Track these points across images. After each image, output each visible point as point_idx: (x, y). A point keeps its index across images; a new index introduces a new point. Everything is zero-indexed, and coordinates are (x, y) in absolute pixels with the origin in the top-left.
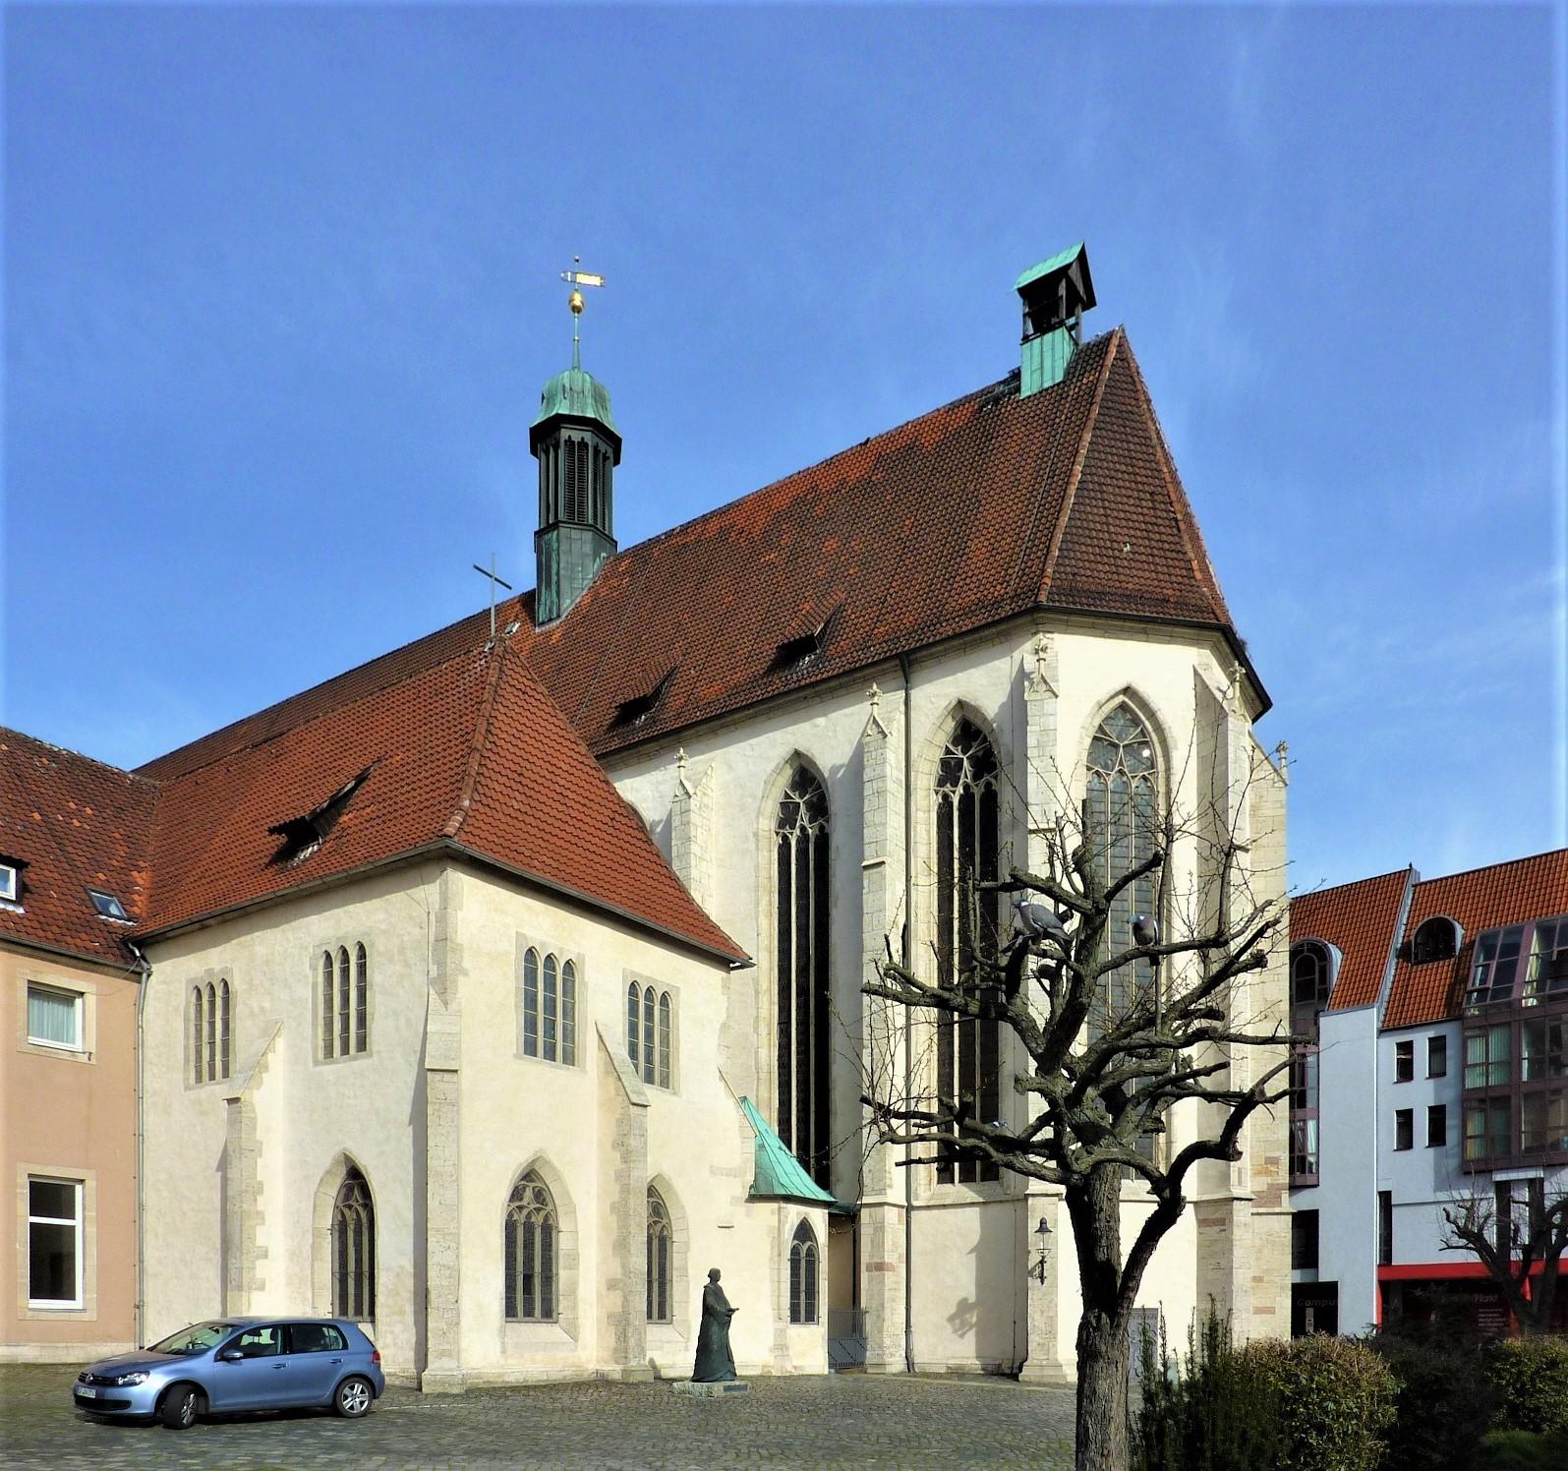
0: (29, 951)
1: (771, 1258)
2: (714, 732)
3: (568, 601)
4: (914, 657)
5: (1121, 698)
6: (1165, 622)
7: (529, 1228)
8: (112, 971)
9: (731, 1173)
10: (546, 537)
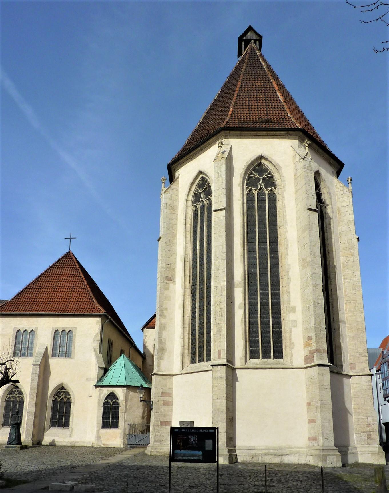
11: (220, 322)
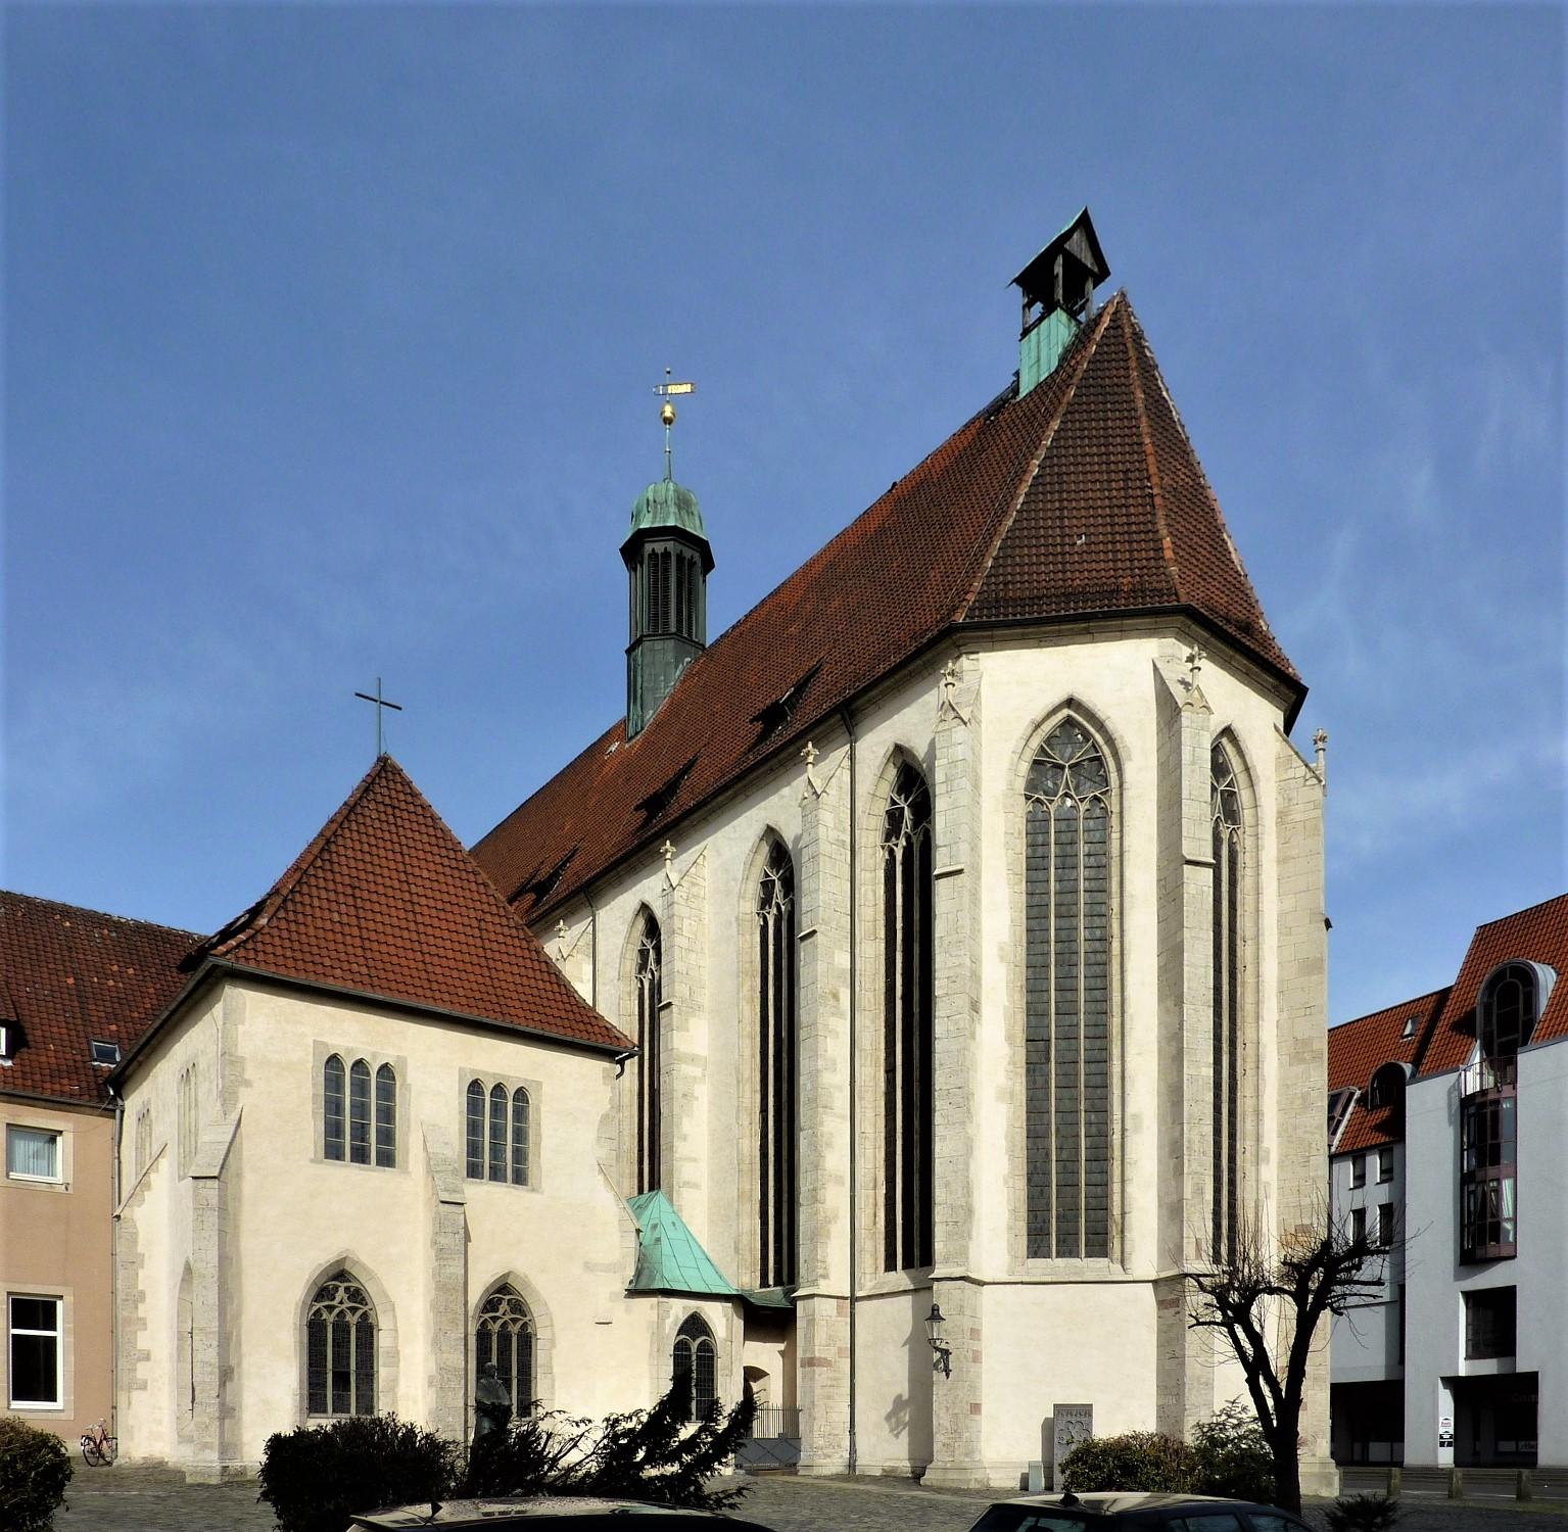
0: (43, 1104)
1: (650, 1355)
2: (705, 819)
3: (651, 712)
4: (854, 706)
5: (1066, 712)
6: (1108, 616)
7: (504, 1337)
8: (88, 1110)
9: (611, 1268)
10: (634, 654)
11: (1199, 1169)
